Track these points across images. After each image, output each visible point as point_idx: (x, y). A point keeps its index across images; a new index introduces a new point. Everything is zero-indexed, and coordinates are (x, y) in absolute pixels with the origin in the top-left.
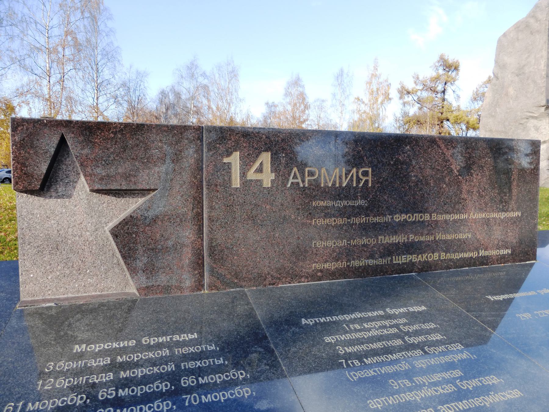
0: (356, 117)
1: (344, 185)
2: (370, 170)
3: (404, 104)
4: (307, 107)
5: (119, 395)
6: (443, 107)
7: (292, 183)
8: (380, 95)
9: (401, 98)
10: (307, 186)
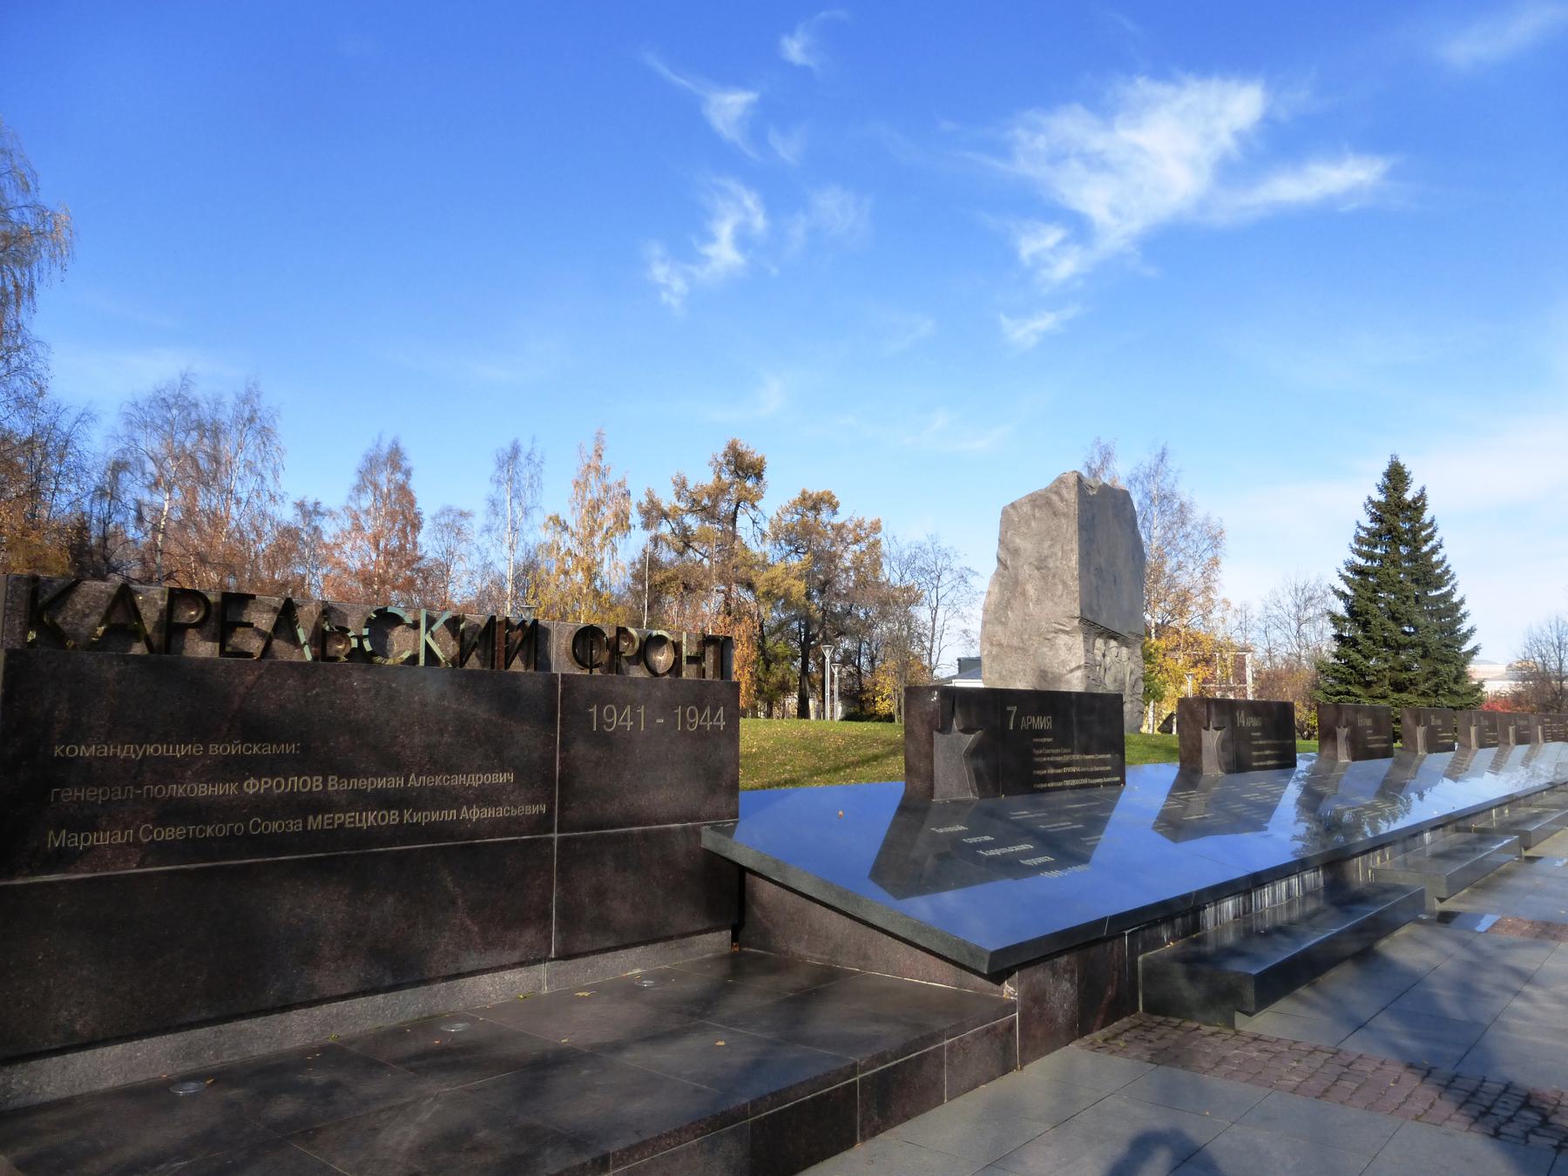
4: (416, 526)
8: (604, 513)
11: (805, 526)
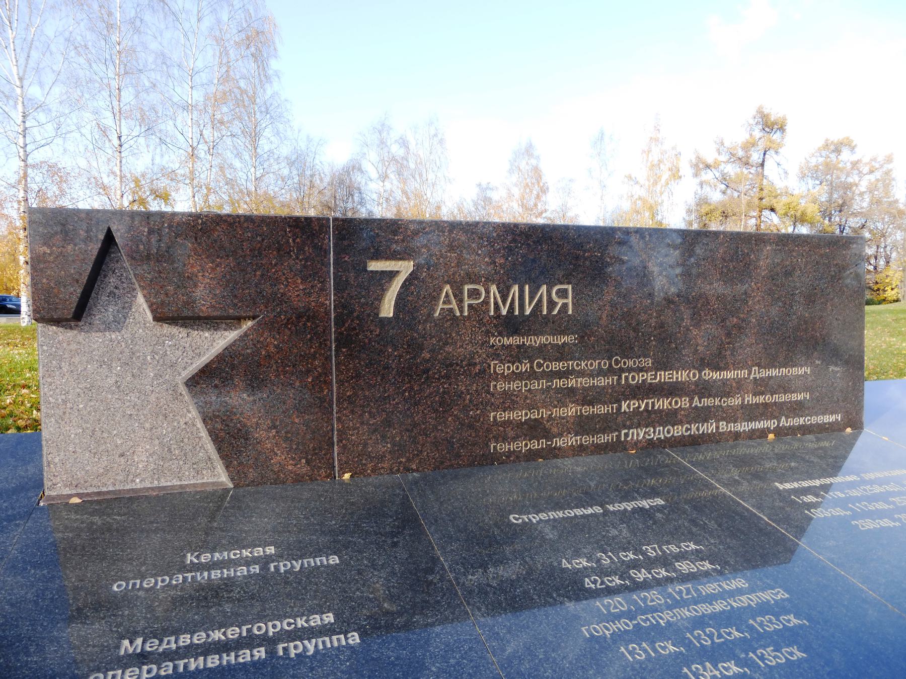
0: (626, 206)
1: (528, 312)
2: (570, 287)
3: (701, 184)
4: (544, 190)
5: (256, 658)
6: (762, 189)
7: (470, 306)
8: (665, 172)
9: (696, 175)
10: (466, 314)
11: (827, 165)
